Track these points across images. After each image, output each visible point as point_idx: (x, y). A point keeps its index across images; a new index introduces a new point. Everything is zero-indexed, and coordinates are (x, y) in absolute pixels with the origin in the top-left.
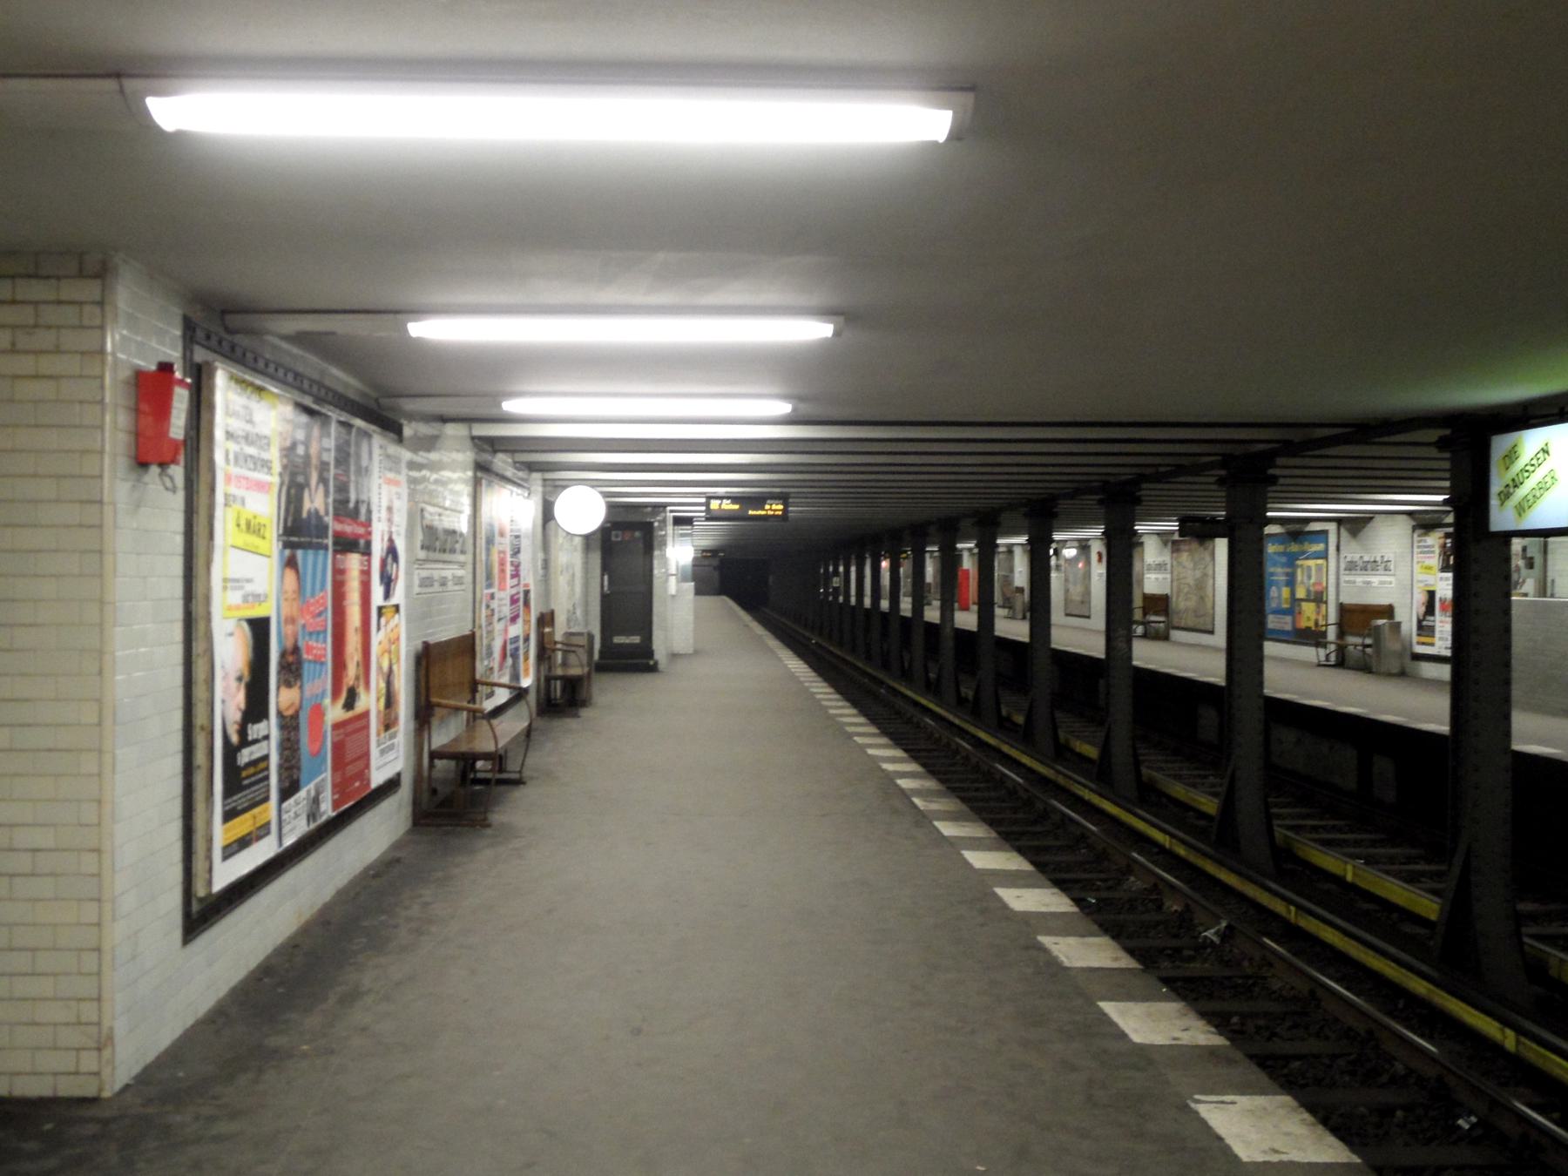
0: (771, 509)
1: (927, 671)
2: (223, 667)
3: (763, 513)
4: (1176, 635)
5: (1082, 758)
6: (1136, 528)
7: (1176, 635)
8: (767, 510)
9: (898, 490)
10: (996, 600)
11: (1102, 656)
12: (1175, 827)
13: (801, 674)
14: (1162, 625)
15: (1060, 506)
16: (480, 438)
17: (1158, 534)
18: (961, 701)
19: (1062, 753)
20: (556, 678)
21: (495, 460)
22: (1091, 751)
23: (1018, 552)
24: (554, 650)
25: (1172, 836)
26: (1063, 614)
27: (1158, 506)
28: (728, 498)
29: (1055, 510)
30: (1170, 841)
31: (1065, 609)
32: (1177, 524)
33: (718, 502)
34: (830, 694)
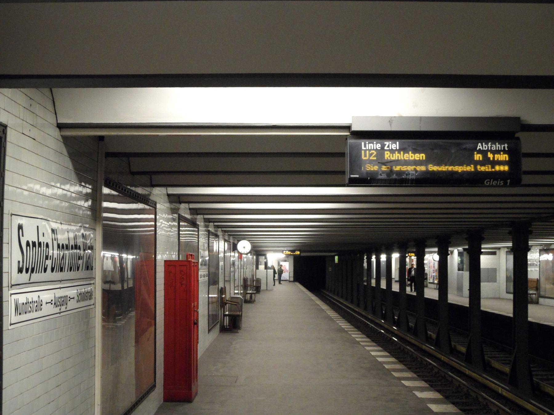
0: (486, 161)
1: (408, 322)
2: (213, 280)
3: (470, 168)
4: (541, 300)
5: (502, 373)
6: (482, 247)
7: (541, 300)
8: (476, 163)
9: (399, 226)
10: (393, 276)
11: (437, 299)
12: (543, 406)
13: (333, 315)
14: (534, 296)
15: (533, 227)
16: (216, 225)
17: (507, 248)
18: (409, 329)
19: (453, 352)
20: (226, 315)
21: (218, 233)
22: (463, 349)
23: (531, 255)
24: (247, 287)
25: (419, 342)
26: (505, 292)
27: (550, 228)
28: (287, 250)
29: (426, 243)
30: (501, 390)
31: (506, 291)
32: (512, 244)
33: (285, 251)
34: (336, 315)
